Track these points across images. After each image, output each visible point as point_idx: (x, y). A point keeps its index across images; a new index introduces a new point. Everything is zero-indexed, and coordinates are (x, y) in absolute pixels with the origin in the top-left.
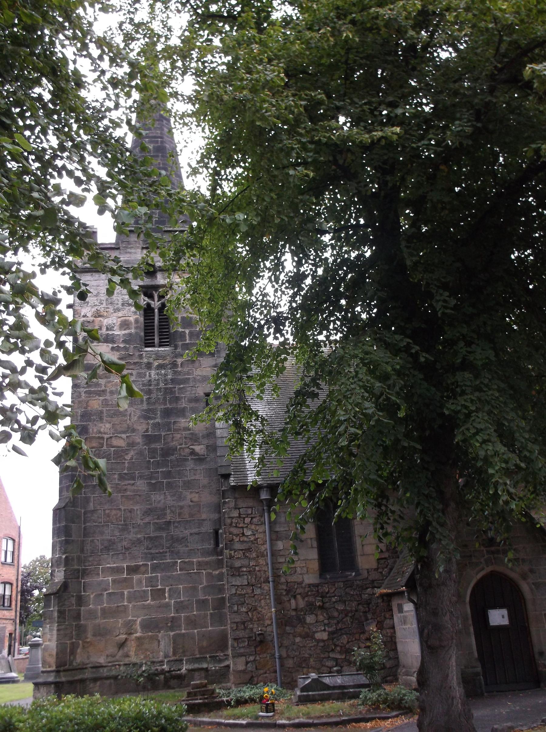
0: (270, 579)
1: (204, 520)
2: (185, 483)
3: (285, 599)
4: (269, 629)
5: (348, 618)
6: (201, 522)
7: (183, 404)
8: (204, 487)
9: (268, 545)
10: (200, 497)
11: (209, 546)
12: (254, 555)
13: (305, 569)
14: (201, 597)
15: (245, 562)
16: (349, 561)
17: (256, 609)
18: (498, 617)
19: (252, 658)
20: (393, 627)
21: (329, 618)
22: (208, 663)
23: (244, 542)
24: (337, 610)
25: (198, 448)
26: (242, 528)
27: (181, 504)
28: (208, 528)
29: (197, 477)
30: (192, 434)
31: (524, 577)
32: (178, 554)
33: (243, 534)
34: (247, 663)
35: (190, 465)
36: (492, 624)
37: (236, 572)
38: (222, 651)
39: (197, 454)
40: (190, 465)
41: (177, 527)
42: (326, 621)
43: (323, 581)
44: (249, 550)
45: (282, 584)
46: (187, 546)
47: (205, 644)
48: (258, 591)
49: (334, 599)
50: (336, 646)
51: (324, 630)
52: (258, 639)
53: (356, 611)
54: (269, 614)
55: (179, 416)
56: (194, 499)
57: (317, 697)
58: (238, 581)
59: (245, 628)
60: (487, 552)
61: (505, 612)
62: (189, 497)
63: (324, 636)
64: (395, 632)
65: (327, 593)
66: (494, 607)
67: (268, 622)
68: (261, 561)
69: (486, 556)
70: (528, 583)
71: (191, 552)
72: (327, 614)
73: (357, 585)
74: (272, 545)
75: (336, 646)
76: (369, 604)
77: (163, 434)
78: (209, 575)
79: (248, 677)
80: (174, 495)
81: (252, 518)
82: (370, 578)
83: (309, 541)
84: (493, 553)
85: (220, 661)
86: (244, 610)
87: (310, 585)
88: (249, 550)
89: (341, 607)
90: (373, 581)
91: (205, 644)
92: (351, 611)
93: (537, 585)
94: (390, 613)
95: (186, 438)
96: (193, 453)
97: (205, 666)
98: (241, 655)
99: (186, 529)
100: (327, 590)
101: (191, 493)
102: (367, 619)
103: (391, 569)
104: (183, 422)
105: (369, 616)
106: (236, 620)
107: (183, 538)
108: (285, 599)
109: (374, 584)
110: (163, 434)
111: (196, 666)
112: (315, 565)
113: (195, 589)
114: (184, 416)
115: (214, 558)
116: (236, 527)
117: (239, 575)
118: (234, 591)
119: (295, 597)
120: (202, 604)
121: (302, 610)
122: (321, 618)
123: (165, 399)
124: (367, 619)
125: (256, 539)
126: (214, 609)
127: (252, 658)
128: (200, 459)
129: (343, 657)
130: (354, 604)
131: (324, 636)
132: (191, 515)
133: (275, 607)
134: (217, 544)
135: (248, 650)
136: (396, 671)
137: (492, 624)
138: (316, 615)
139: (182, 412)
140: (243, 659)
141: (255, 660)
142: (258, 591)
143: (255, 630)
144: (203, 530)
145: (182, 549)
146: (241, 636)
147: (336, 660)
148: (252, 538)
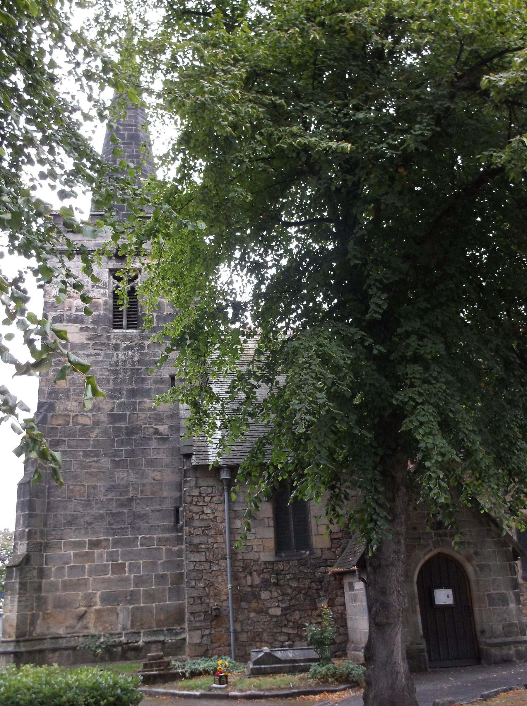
1: (165, 498)
2: (148, 461)
3: (242, 575)
4: (225, 604)
5: (301, 595)
6: (162, 499)
7: (149, 385)
8: (167, 465)
9: (226, 524)
10: (162, 475)
11: (171, 523)
12: (213, 532)
13: (261, 547)
15: (204, 539)
16: (304, 540)
17: (213, 585)
18: (443, 597)
19: (207, 632)
20: (344, 604)
21: (284, 594)
22: (165, 635)
24: (291, 587)
25: (163, 429)
26: (202, 506)
27: (144, 481)
28: (168, 505)
29: (160, 456)
30: (156, 414)
32: (139, 530)
33: (203, 512)
34: (203, 636)
35: (154, 444)
37: (195, 548)
38: (179, 624)
39: (161, 434)
40: (154, 444)
41: (138, 504)
42: (280, 598)
43: (278, 559)
44: (208, 527)
46: (148, 523)
47: (162, 617)
49: (288, 577)
50: (289, 621)
51: (278, 606)
52: (214, 613)
53: (309, 588)
54: (225, 590)
55: (143, 396)
56: (157, 478)
58: (196, 557)
59: (202, 603)
60: (435, 534)
61: (450, 592)
62: (151, 475)
63: (278, 612)
64: (345, 609)
65: (282, 570)
66: (440, 587)
68: (220, 539)
69: (434, 539)
70: (472, 565)
71: (152, 529)
72: (281, 591)
73: (311, 564)
74: (230, 523)
75: (289, 621)
76: (321, 582)
77: (128, 413)
78: (169, 550)
79: (203, 649)
80: (136, 474)
81: (212, 497)
82: (324, 557)
83: (266, 520)
84: (440, 535)
85: (177, 634)
86: (201, 585)
87: (265, 563)
88: (208, 527)
89: (294, 584)
90: (326, 560)
91: (162, 617)
92: (304, 589)
93: (481, 567)
94: (341, 591)
95: (150, 418)
96: (157, 432)
97: (162, 638)
98: (198, 629)
99: (147, 506)
100: (282, 568)
101: (154, 471)
102: (319, 596)
103: (344, 549)
104: (149, 403)
105: (322, 593)
106: (194, 595)
107: (145, 515)
108: (242, 575)
109: (327, 563)
110: (128, 413)
111: (154, 638)
112: (271, 544)
113: (154, 564)
114: (149, 397)
115: (174, 534)
116: (196, 505)
117: (198, 552)
118: (192, 568)
120: (162, 578)
121: (257, 586)
122: (275, 594)
123: (131, 380)
124: (319, 596)
125: (215, 518)
126: (172, 584)
127: (207, 632)
128: (164, 439)
129: (295, 632)
130: (307, 582)
131: (278, 612)
132: (153, 493)
133: (231, 583)
134: (177, 521)
135: (203, 624)
136: (346, 646)
138: (271, 592)
139: (147, 393)
140: (200, 631)
141: (210, 634)
142: (215, 568)
143: (211, 605)
144: (164, 507)
145: (143, 525)
146: (198, 610)
147: (289, 635)
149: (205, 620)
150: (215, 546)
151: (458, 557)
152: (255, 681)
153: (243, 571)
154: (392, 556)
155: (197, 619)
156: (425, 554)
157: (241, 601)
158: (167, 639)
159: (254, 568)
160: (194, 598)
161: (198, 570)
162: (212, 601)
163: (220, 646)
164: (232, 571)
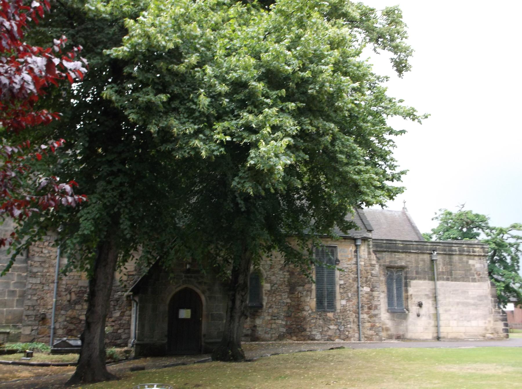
0: (56, 281)
4: (50, 311)
9: (57, 261)
12: (47, 265)
14: (12, 288)
15: (40, 269)
17: (43, 299)
18: (185, 314)
19: (35, 328)
22: (10, 328)
23: (41, 257)
26: (42, 248)
31: (204, 292)
33: (42, 252)
34: (32, 330)
36: (189, 317)
37: (34, 275)
44: (44, 262)
45: (63, 285)
47: (10, 317)
48: (46, 288)
52: (41, 317)
54: (51, 302)
57: (120, 357)
58: (34, 281)
59: (34, 310)
60: (185, 276)
61: (189, 311)
67: (50, 307)
68: (52, 270)
69: (184, 279)
70: (205, 296)
74: (60, 261)
76: (118, 301)
78: (19, 275)
79: (32, 338)
81: (50, 243)
84: (188, 277)
86: (35, 298)
88: (44, 262)
97: (8, 331)
98: (29, 325)
102: (115, 310)
106: (29, 304)
116: (38, 247)
117: (35, 277)
119: (70, 293)
125: (50, 256)
127: (35, 328)
135: (34, 323)
136: (127, 341)
137: (189, 317)
140: (30, 328)
141: (37, 329)
143: (40, 311)
146: (31, 314)
148: (48, 255)
149: (35, 320)
150: (48, 274)
151: (198, 291)
152: (51, 356)
153: (65, 291)
154: (102, 285)
155: (30, 319)
156: (176, 288)
157: (62, 310)
158: (12, 331)
159: (73, 290)
160: (29, 306)
161: (34, 289)
162: (41, 308)
163: (43, 337)
164: (57, 291)
